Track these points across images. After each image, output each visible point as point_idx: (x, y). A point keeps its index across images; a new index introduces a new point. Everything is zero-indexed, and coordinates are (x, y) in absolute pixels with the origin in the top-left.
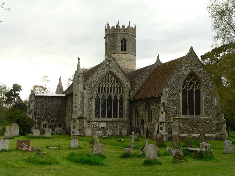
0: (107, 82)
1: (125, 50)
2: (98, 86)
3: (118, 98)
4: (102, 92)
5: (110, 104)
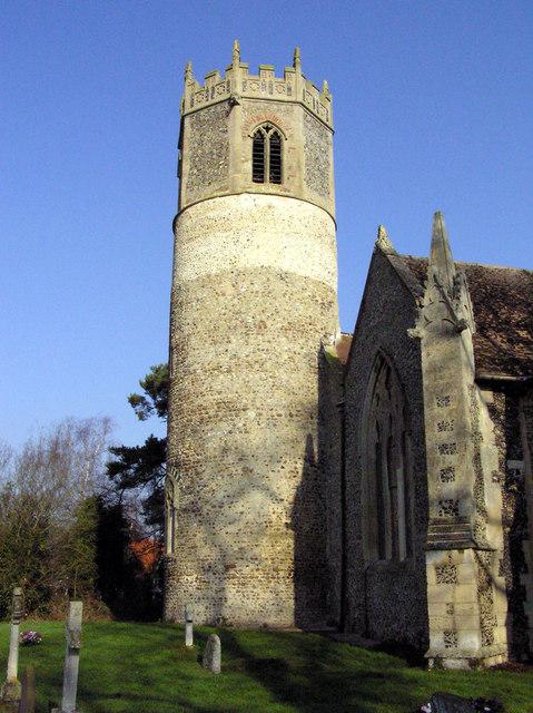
1: (277, 179)
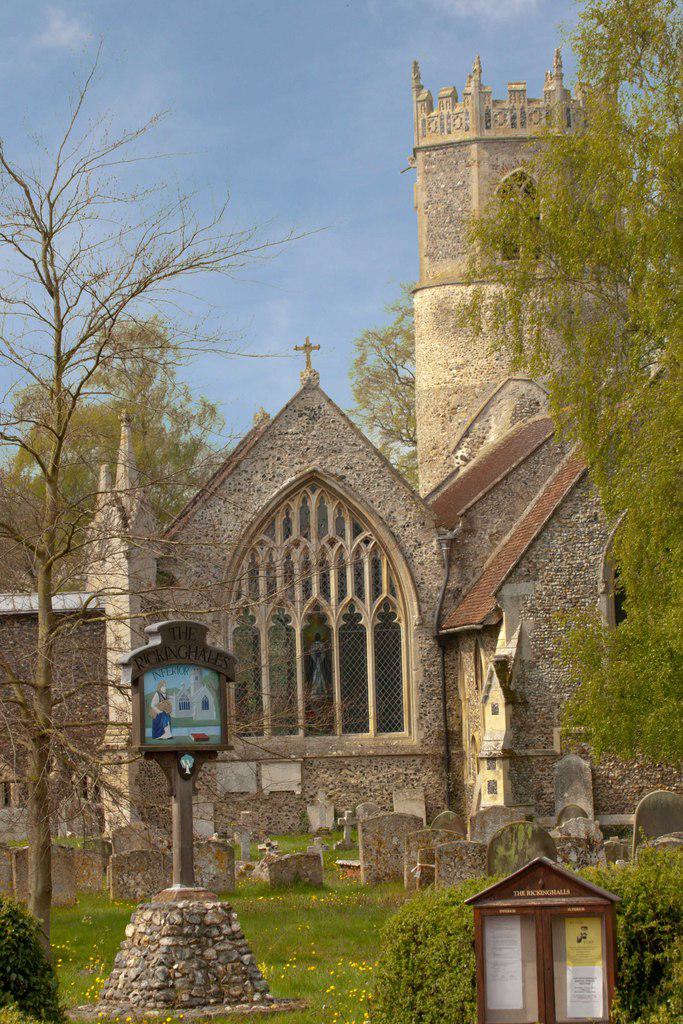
0: (295, 533)
2: (245, 564)
3: (367, 621)
4: (342, 593)
5: (323, 656)
